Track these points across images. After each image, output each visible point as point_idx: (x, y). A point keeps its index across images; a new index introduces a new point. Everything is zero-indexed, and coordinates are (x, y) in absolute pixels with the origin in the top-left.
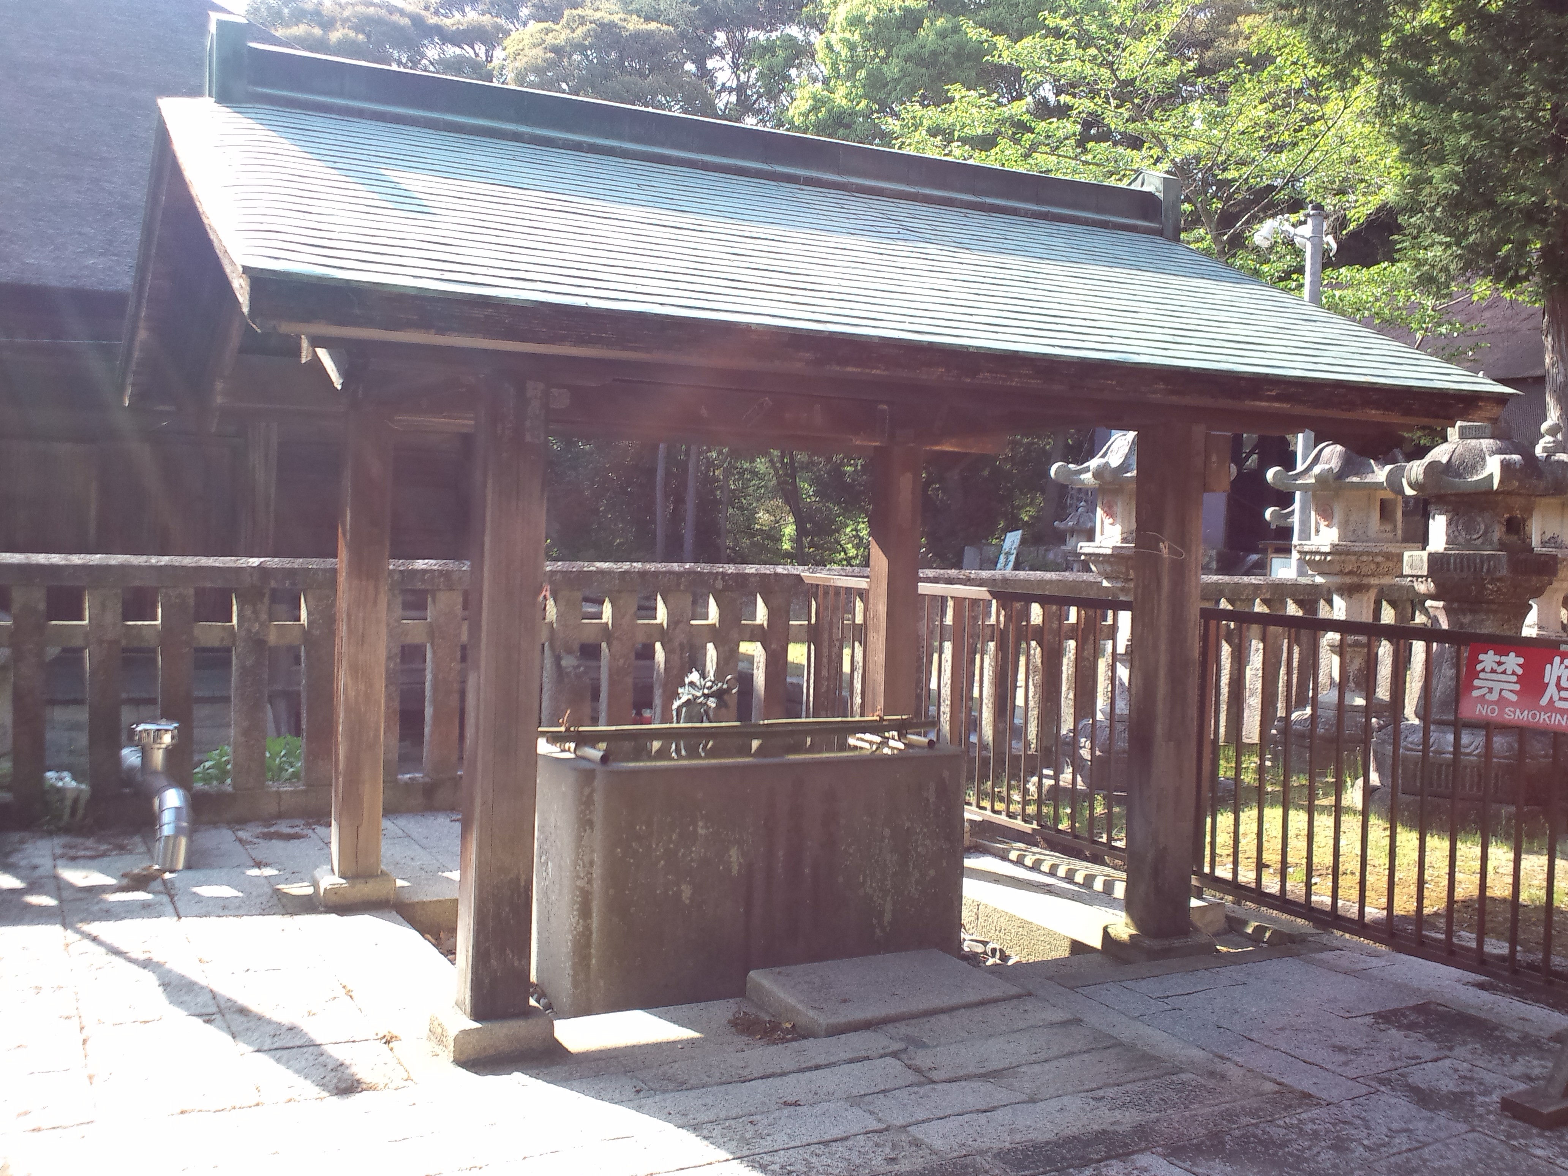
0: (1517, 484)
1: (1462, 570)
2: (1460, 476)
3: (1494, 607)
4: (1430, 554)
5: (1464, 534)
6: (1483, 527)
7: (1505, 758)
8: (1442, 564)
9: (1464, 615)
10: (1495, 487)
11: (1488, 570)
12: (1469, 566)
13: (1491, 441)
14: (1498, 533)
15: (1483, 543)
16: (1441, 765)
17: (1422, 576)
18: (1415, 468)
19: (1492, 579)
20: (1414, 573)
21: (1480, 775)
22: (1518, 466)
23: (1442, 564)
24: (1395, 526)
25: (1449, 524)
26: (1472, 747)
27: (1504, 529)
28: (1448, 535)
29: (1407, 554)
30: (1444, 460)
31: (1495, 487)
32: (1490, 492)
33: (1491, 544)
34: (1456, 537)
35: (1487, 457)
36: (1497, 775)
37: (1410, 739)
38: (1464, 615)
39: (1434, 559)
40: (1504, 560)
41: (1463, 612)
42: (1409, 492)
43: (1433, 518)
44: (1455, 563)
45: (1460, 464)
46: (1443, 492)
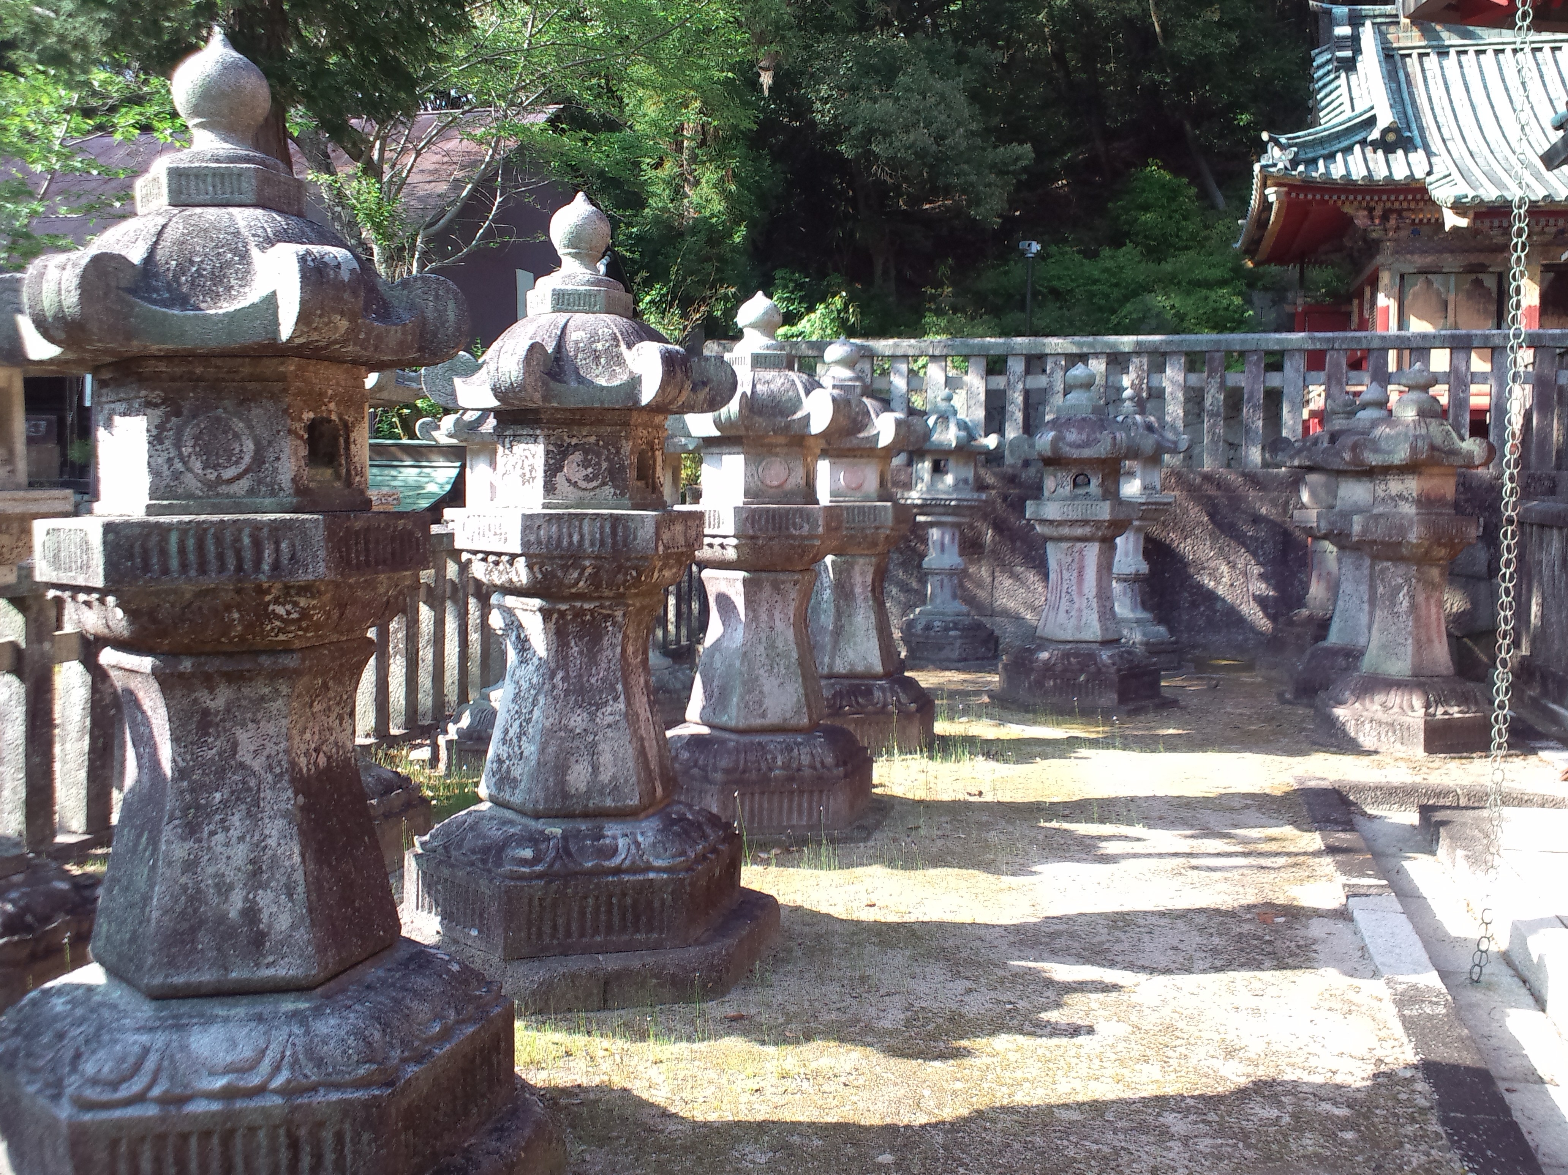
0: (343, 324)
1: (203, 570)
2: (183, 301)
3: (291, 662)
4: (109, 528)
5: (197, 465)
6: (249, 446)
7: (358, 1084)
8: (145, 552)
9: (211, 690)
10: (286, 330)
11: (276, 566)
12: (221, 557)
13: (259, 212)
14: (289, 462)
15: (251, 492)
16: (184, 1137)
17: (89, 590)
18: (52, 274)
19: (287, 588)
20: (65, 578)
21: (294, 1145)
22: (345, 276)
23: (145, 552)
24: (11, 452)
25: (156, 439)
26: (265, 1067)
27: (303, 451)
28: (154, 471)
29: (40, 527)
30: (136, 255)
31: (286, 330)
32: (276, 351)
33: (273, 494)
34: (177, 476)
35: (255, 252)
36: (339, 1137)
37: (89, 1068)
38: (211, 690)
39: (120, 540)
40: (318, 536)
41: (209, 682)
42: (39, 349)
43: (109, 425)
44: (182, 550)
45: (182, 269)
46: (135, 346)
